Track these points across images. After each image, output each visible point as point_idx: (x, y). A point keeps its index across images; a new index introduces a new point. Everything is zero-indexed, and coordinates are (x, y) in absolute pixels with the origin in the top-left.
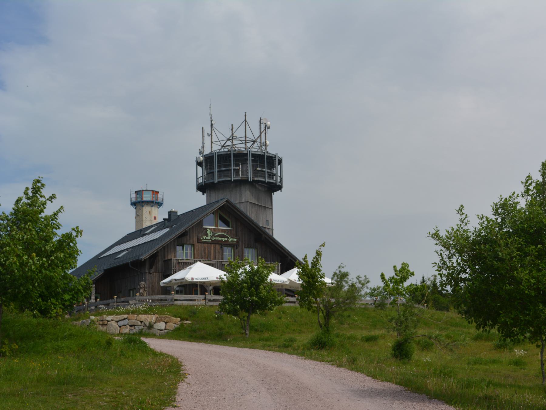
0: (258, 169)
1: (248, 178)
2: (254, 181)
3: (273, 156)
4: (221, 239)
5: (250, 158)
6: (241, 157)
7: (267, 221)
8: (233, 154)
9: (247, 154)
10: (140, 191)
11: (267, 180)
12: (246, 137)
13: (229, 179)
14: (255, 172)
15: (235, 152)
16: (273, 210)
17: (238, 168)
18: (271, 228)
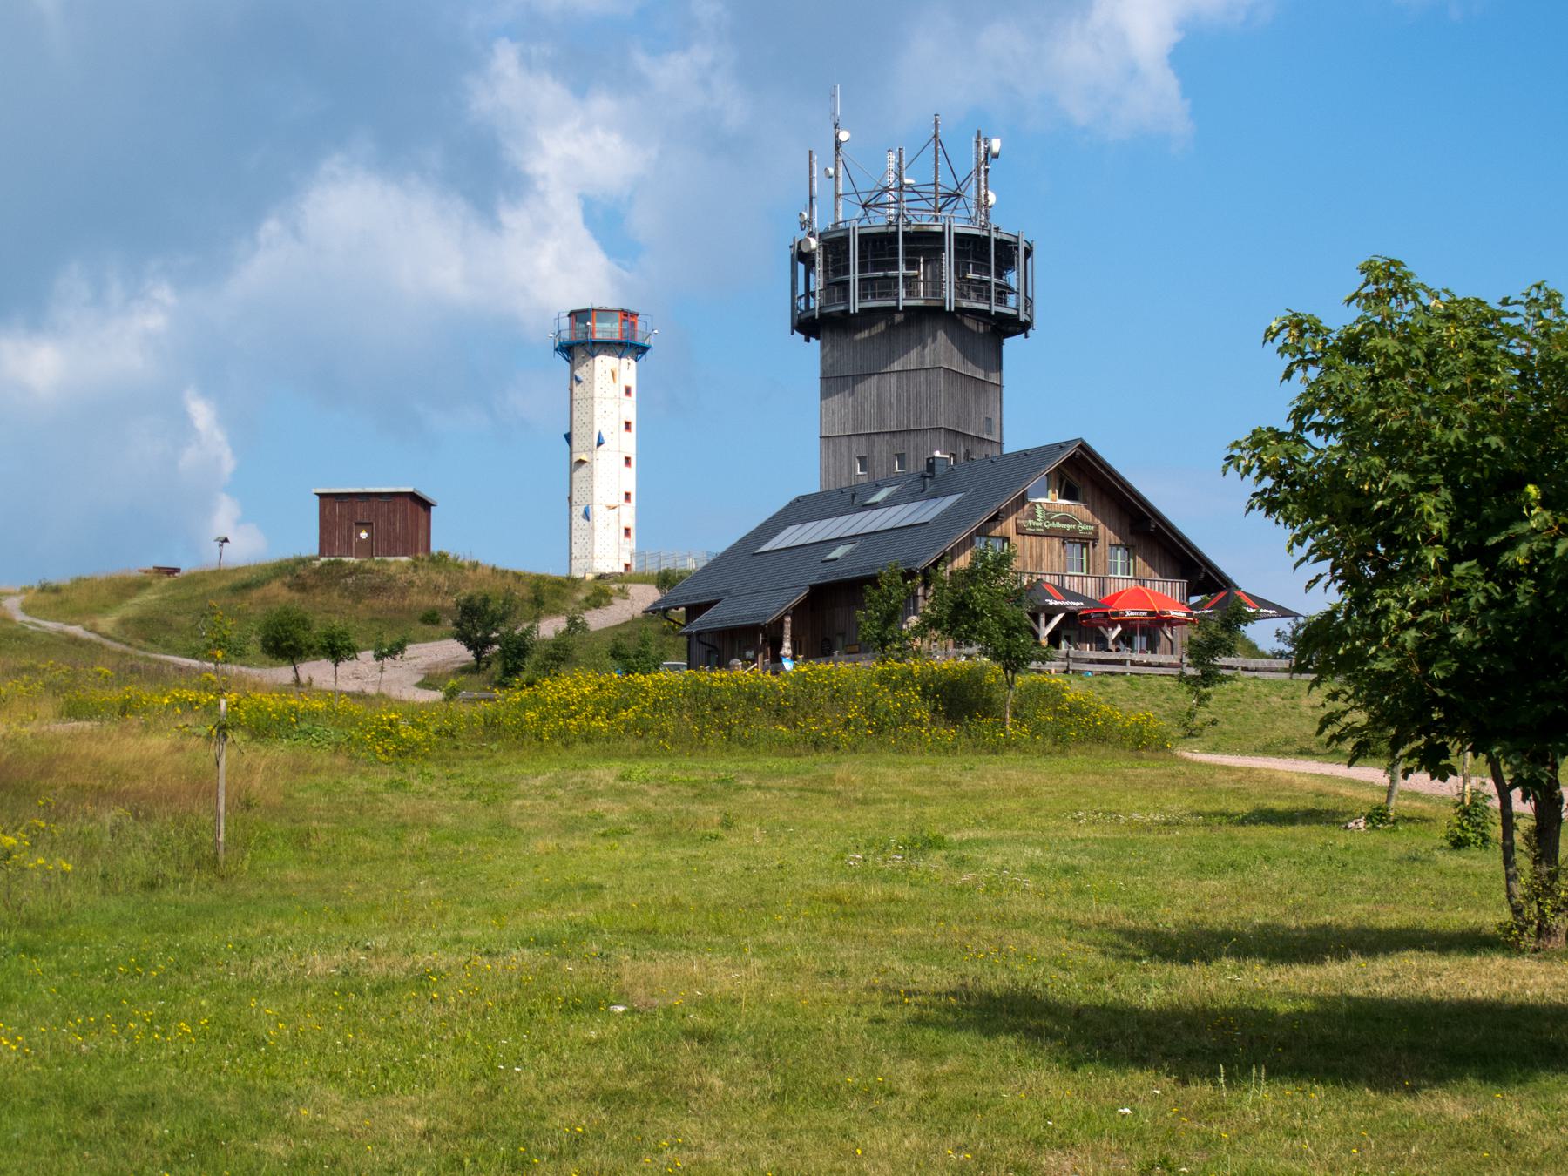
0: (970, 275)
1: (944, 301)
2: (959, 310)
3: (1013, 239)
4: (1063, 526)
5: (950, 245)
6: (925, 244)
7: (989, 419)
8: (904, 233)
9: (942, 234)
10: (586, 311)
11: (995, 309)
12: (935, 184)
13: (893, 303)
14: (964, 287)
15: (908, 229)
16: (1005, 391)
17: (916, 272)
18: (997, 440)
